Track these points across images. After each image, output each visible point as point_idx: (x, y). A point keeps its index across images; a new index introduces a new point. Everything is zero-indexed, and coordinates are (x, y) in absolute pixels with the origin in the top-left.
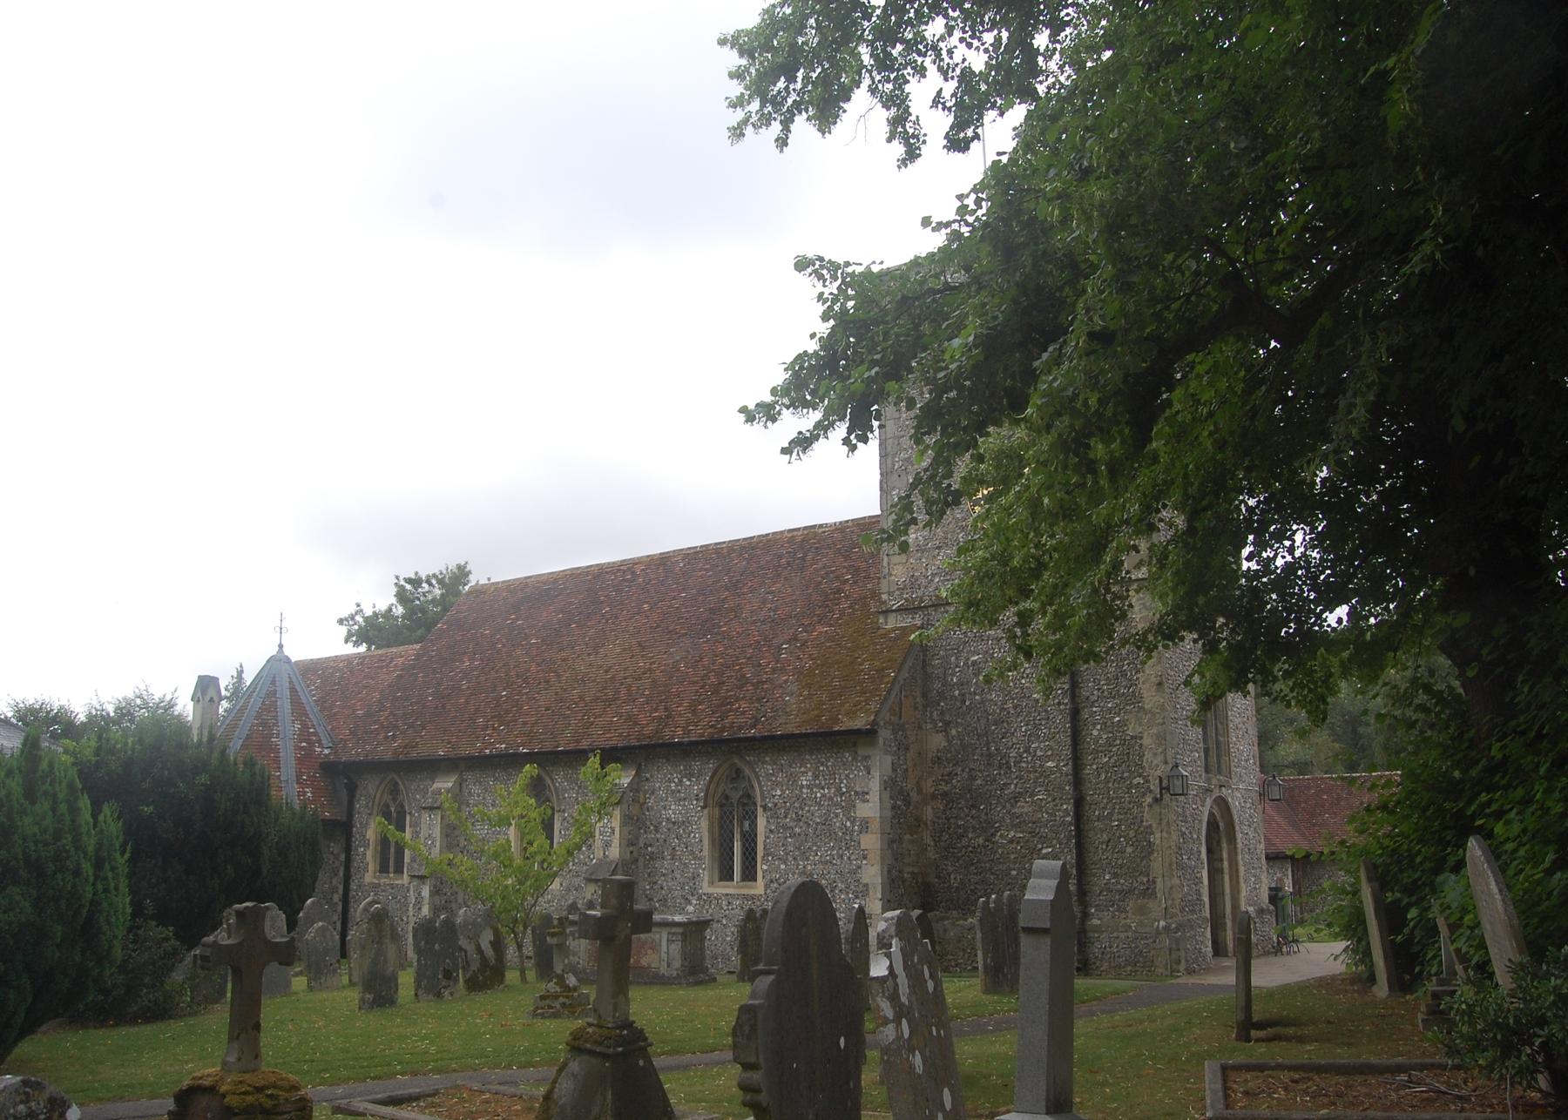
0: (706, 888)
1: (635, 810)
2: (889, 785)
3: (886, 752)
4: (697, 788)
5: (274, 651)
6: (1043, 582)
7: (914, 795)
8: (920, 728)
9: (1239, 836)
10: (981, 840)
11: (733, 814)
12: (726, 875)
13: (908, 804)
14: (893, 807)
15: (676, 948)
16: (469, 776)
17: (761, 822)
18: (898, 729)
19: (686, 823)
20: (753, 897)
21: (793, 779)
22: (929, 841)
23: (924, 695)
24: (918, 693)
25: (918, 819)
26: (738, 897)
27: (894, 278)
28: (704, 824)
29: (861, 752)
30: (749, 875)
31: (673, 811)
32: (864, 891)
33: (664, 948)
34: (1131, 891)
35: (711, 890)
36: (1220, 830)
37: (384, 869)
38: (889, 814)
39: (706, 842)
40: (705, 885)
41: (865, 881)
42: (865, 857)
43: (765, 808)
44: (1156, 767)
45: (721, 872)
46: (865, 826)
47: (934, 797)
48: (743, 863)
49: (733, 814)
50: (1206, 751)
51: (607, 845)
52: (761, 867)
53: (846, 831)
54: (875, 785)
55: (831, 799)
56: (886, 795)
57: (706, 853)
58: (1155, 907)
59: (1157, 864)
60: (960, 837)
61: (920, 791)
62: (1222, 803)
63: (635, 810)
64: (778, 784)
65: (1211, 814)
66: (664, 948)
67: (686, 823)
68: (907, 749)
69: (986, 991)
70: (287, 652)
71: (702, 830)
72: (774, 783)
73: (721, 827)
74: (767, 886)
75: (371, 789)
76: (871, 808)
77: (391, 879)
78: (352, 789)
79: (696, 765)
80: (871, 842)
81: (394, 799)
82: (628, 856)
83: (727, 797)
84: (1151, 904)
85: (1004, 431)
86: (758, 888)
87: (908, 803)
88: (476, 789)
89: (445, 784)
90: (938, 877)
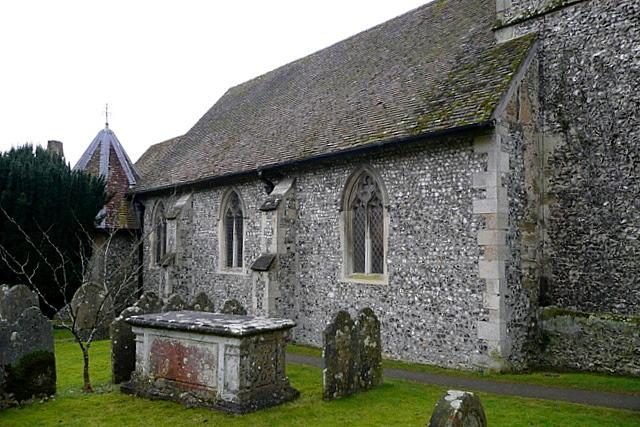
0: (342, 278)
1: (291, 214)
2: (508, 182)
3: (505, 150)
4: (335, 194)
5: (103, 127)
7: (530, 193)
8: (536, 130)
10: (604, 237)
11: (364, 213)
12: (359, 267)
13: (526, 203)
14: (511, 204)
15: (234, 365)
16: (196, 196)
17: (387, 221)
18: (515, 128)
19: (328, 224)
21: (413, 181)
22: (546, 238)
23: (541, 99)
24: (535, 97)
25: (534, 217)
26: (367, 286)
27: (423, 371)
28: (341, 224)
29: (478, 149)
30: (377, 268)
31: (318, 215)
32: (481, 286)
33: (221, 364)
35: (346, 281)
37: (229, 264)
38: (507, 210)
39: (342, 240)
40: (342, 274)
41: (482, 277)
42: (482, 253)
43: (389, 208)
45: (355, 264)
46: (483, 221)
47: (550, 194)
48: (373, 257)
51: (269, 243)
52: (387, 261)
53: (462, 227)
54: (492, 182)
55: (448, 197)
56: (504, 191)
57: (342, 248)
60: (580, 234)
61: (536, 190)
63: (291, 214)
64: (400, 187)
66: (221, 364)
67: (328, 224)
68: (524, 149)
70: (110, 127)
71: (339, 231)
72: (394, 183)
73: (355, 227)
74: (391, 278)
75: (150, 206)
76: (491, 203)
77: (234, 272)
78: (142, 209)
79: (335, 176)
82: (285, 251)
83: (359, 201)
87: (525, 199)
88: (201, 205)
89: (183, 201)
90: (556, 273)
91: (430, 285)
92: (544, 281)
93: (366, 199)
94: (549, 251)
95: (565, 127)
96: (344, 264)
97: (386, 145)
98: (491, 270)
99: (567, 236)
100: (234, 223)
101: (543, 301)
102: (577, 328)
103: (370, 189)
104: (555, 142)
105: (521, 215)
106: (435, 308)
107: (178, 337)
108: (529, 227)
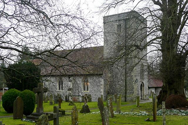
6: (174, 57)
9: (145, 86)
20: (88, 93)
28: (82, 84)
30: (87, 90)
34: (131, 93)
36: (142, 86)
37: (60, 89)
44: (135, 79)
46: (101, 84)
49: (61, 83)
50: (141, 77)
52: (89, 89)
58: (134, 94)
59: (134, 90)
62: (143, 83)
65: (141, 84)
69: (87, 106)
72: (90, 80)
80: (102, 87)
81: (61, 80)
84: (133, 94)
85: (5, 24)
86: (89, 92)
91: (95, 92)
92: (108, 91)
93: (86, 81)
94: (109, 88)
95: (111, 73)
96: (83, 89)
97: (16, 50)
98: (102, 90)
99: (111, 86)
100: (61, 83)
101: (108, 94)
102: (112, 97)
103: (87, 79)
104: (110, 75)
105: (105, 84)
106: (95, 95)
107: (74, 97)
108: (107, 85)
